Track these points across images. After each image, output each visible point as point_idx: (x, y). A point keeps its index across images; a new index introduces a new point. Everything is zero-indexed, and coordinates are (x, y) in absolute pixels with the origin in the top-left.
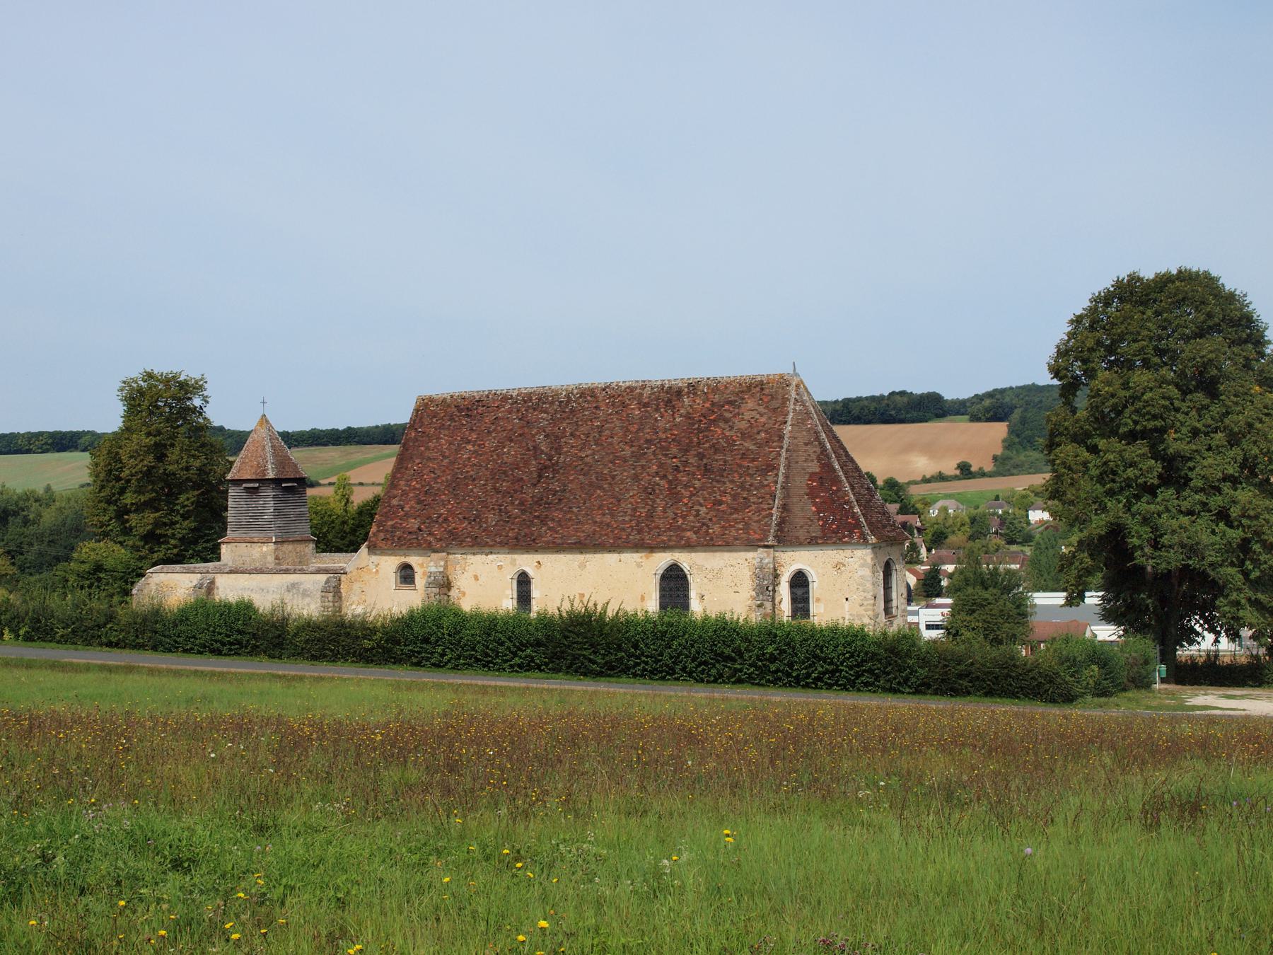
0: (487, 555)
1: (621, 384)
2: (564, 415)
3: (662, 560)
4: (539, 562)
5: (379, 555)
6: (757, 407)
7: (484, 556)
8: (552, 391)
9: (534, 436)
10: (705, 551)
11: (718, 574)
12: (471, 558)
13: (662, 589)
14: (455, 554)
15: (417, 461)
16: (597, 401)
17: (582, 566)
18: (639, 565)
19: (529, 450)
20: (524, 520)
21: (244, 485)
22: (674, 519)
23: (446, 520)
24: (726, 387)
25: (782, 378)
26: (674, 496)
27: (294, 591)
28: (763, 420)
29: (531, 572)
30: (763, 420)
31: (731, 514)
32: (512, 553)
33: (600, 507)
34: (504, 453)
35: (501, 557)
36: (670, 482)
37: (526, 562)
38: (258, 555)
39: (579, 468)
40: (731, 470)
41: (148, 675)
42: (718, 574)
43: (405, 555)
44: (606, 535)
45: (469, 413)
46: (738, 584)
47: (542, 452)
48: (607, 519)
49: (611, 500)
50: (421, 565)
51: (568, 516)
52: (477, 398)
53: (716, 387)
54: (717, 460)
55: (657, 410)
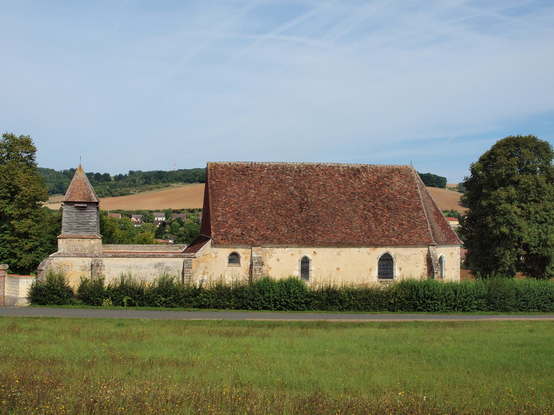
0: (285, 248)
1: (325, 164)
2: (301, 178)
3: (381, 251)
4: (315, 252)
5: (218, 247)
6: (401, 180)
7: (283, 249)
8: (288, 165)
9: (288, 187)
10: (403, 247)
11: (408, 258)
12: (276, 250)
13: (379, 265)
14: (265, 247)
15: (224, 197)
16: (316, 172)
17: (339, 254)
18: (369, 254)
19: (288, 194)
20: (303, 230)
21: (76, 205)
22: (383, 232)
23: (257, 229)
24: (381, 170)
25: (407, 167)
26: (377, 220)
27: (160, 267)
28: (406, 186)
29: (310, 256)
30: (406, 186)
31: (410, 230)
32: (300, 247)
33: (342, 225)
34: (275, 195)
35: (293, 249)
36: (373, 214)
37: (308, 252)
38: (87, 246)
39: (321, 205)
40: (401, 209)
41: (317, 328)
42: (408, 258)
43: (234, 248)
44: (352, 239)
45: (244, 173)
46: (418, 263)
47: (297, 196)
48: (349, 231)
49: (346, 222)
50: (244, 253)
51: (327, 229)
52: (245, 166)
53: (376, 170)
54: (391, 204)
55: (350, 178)
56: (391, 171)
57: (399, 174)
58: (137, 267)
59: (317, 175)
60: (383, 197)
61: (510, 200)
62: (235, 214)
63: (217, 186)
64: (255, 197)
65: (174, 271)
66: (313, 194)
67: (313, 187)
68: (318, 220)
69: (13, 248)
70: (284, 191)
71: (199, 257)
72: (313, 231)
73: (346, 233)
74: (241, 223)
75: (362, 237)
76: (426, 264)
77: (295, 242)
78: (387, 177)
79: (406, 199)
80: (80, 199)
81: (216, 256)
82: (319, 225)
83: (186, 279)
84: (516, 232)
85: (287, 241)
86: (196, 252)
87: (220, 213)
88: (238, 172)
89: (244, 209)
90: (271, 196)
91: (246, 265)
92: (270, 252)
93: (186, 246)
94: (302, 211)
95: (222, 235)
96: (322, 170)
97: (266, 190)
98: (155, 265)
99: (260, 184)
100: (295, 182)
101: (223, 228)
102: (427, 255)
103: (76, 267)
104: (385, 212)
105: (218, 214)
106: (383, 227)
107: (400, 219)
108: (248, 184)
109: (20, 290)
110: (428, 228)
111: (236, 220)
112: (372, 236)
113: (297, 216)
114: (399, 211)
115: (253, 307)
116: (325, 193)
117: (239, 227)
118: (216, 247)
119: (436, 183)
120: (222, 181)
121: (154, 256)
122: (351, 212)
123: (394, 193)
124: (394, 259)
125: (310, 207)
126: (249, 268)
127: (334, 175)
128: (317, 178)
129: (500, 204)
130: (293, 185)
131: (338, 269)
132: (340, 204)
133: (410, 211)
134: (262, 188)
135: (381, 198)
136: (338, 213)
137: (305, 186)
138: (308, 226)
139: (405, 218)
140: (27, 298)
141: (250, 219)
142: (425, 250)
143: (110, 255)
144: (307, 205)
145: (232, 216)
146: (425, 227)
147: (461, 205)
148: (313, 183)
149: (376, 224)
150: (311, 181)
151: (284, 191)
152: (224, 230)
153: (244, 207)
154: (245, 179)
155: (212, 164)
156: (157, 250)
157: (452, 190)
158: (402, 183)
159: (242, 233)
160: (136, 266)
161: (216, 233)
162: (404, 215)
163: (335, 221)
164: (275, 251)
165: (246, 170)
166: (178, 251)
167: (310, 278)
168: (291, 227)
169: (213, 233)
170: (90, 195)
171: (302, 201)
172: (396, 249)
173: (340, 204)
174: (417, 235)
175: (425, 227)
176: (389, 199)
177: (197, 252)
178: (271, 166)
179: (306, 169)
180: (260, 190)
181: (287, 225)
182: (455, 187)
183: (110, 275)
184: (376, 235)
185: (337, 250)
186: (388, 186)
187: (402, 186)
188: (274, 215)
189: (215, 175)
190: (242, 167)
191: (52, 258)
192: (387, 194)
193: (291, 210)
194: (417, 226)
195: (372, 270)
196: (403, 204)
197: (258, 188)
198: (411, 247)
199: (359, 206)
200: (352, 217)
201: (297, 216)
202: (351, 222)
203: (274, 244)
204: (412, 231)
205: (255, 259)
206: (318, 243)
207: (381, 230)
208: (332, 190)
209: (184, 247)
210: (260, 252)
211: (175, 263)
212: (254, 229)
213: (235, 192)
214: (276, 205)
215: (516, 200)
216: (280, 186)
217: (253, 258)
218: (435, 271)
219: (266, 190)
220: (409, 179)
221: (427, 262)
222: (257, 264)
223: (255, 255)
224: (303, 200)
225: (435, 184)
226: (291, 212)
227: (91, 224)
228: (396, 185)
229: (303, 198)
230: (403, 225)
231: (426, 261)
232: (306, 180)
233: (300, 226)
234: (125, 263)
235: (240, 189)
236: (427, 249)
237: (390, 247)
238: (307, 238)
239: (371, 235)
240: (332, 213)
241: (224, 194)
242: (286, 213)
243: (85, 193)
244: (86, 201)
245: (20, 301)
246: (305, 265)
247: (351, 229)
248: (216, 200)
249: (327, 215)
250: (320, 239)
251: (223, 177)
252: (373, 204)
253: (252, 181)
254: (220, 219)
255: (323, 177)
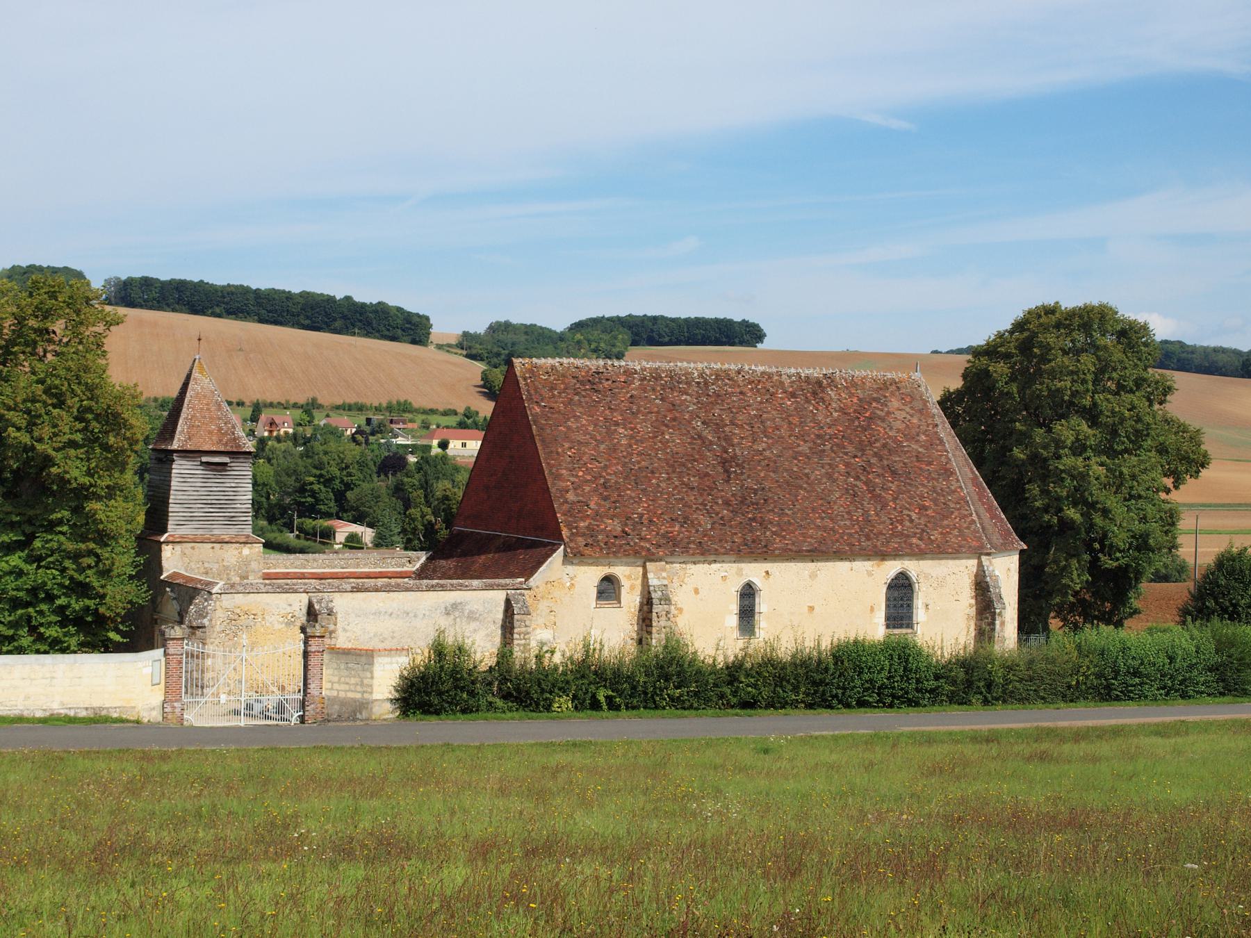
0: (710, 563)
3: (892, 568)
4: (767, 573)
5: (576, 564)
7: (706, 566)
9: (690, 422)
10: (932, 559)
12: (693, 569)
14: (672, 563)
15: (567, 445)
16: (739, 386)
17: (813, 576)
19: (692, 438)
20: (741, 523)
21: (204, 459)
24: (864, 383)
26: (876, 498)
27: (457, 614)
29: (758, 582)
32: (739, 562)
34: (668, 441)
36: (865, 483)
37: (753, 572)
38: (233, 561)
43: (609, 565)
44: (837, 541)
47: (711, 443)
49: (820, 502)
50: (629, 577)
54: (896, 462)
55: (807, 401)
56: (882, 386)
58: (408, 614)
59: (741, 393)
60: (878, 445)
61: (1079, 448)
62: (599, 487)
63: (548, 419)
64: (631, 446)
65: (486, 621)
66: (742, 438)
67: (740, 423)
68: (765, 500)
69: (81, 570)
70: (685, 432)
71: (537, 587)
73: (824, 529)
74: (616, 508)
75: (856, 536)
76: (973, 594)
77: (731, 550)
78: (877, 400)
79: (920, 450)
80: (213, 444)
81: (573, 584)
82: (770, 511)
83: (517, 639)
84: (1098, 520)
85: (716, 547)
86: (531, 574)
87: (569, 483)
88: (583, 383)
89: (615, 473)
90: (660, 442)
91: (632, 605)
92: (681, 573)
93: (423, 557)
94: (729, 477)
95: (583, 535)
96: (751, 382)
97: (648, 428)
98: (446, 608)
99: (633, 413)
100: (700, 408)
101: (583, 519)
102: (976, 576)
103: (273, 617)
104: (888, 481)
105: (564, 484)
106: (889, 513)
107: (918, 495)
108: (607, 412)
109: (375, 682)
110: (971, 515)
111: (606, 499)
112: (875, 534)
113: (722, 491)
114: (912, 476)
115: (840, 702)
116: (766, 436)
117: (614, 516)
118: (572, 564)
119: (403, 330)
121: (442, 586)
122: (824, 480)
123: (896, 437)
124: (917, 585)
125: (744, 468)
126: (637, 608)
128: (742, 399)
129: (1059, 457)
130: (697, 416)
131: (811, 608)
132: (799, 461)
133: (933, 479)
134: (639, 423)
135: (875, 447)
136: (800, 482)
137: (722, 420)
140: (391, 700)
141: (631, 497)
142: (972, 564)
143: (349, 589)
144: (737, 465)
145: (595, 490)
147: (484, 394)
148: (737, 413)
150: (734, 407)
151: (685, 432)
152: (587, 524)
153: (614, 469)
155: (523, 365)
156: (358, 566)
157: (448, 351)
158: (907, 413)
159: (623, 531)
160: (405, 612)
161: (570, 530)
162: (923, 485)
163: (798, 500)
164: (691, 572)
165: (597, 380)
166: (405, 569)
167: (757, 630)
168: (717, 514)
169: (565, 533)
170: (233, 434)
171: (725, 455)
172: (921, 562)
173: (799, 461)
174: (956, 532)
175: (966, 513)
177: (535, 576)
178: (645, 370)
179: (717, 379)
180: (635, 428)
181: (707, 509)
182: (453, 342)
183: (348, 634)
184: (881, 533)
185: (811, 566)
186: (883, 420)
187: (909, 421)
188: (676, 486)
189: (536, 389)
190: (588, 372)
191: (219, 596)
192: (885, 439)
193: (707, 475)
194: (952, 512)
196: (918, 461)
197: (630, 423)
198: (947, 558)
199: (837, 466)
200: (829, 491)
201: (722, 491)
202: (829, 503)
203: (693, 555)
204: (946, 522)
205: (655, 591)
206: (777, 552)
207: (888, 522)
208: (778, 429)
209: (419, 558)
210: (664, 574)
211: (488, 603)
213: (586, 432)
214: (675, 464)
215: (1091, 448)
216: (674, 419)
217: (652, 588)
218: (998, 611)
219: (648, 428)
220: (918, 405)
221: (976, 589)
222: (662, 602)
223: (653, 581)
224: (726, 452)
225: (399, 332)
226: (708, 480)
227: (239, 506)
228: (896, 418)
229: (724, 447)
230: (926, 510)
231: (973, 587)
232: (723, 406)
233: (732, 512)
234: (381, 605)
235: (596, 425)
236: (975, 562)
237: (908, 558)
238: (753, 541)
239: (871, 531)
241: (567, 438)
242: (700, 484)
244: (229, 449)
245: (377, 708)
247: (832, 519)
248: (552, 452)
249: (779, 486)
251: (554, 396)
252: (863, 461)
253: (615, 405)
254: (571, 496)
255: (754, 399)
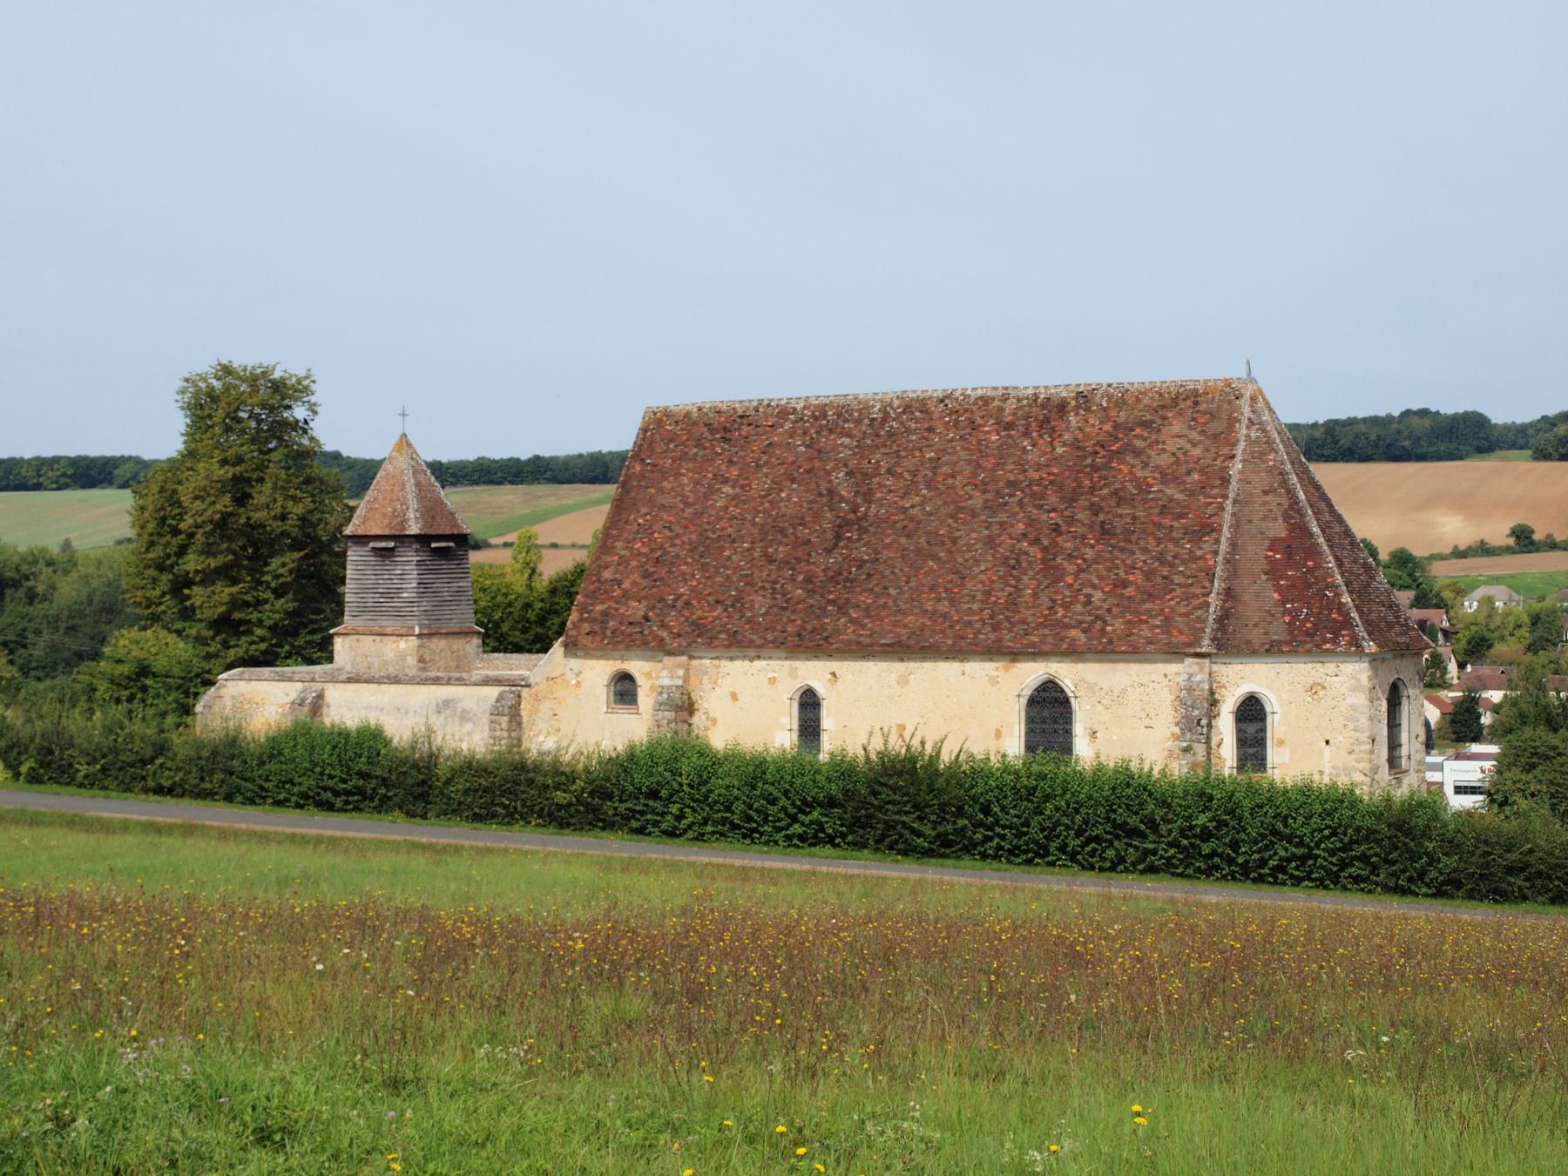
0: (751, 660)
1: (969, 392)
2: (878, 441)
3: (1031, 674)
4: (834, 674)
6: (1187, 432)
7: (747, 663)
8: (859, 402)
9: (829, 473)
10: (1100, 661)
12: (727, 665)
13: (1030, 720)
14: (701, 658)
15: (644, 510)
17: (903, 681)
18: (993, 681)
19: (820, 495)
20: (812, 606)
21: (372, 545)
23: (688, 603)
27: (448, 712)
28: (1197, 452)
29: (821, 689)
30: (1197, 452)
31: (1143, 602)
34: (782, 500)
35: (774, 664)
36: (1045, 550)
37: (814, 673)
39: (899, 525)
42: (1120, 698)
43: (622, 659)
46: (1152, 715)
47: (842, 499)
48: (944, 607)
50: (648, 675)
52: (740, 412)
53: (1121, 399)
54: (1121, 516)
57: (1189, 412)
60: (1105, 492)
72: (840, 608)
85: (755, 637)
92: (713, 672)
110: (1207, 595)
120: (661, 462)
127: (980, 426)
135: (1096, 496)
138: (831, 592)
139: (1145, 561)
146: (1199, 591)
149: (1039, 585)
154: (720, 454)
176: (1120, 499)
184: (1024, 621)
186: (1137, 453)
195: (1004, 734)
198: (1128, 661)
204: (1148, 606)
212: (679, 604)
216: (808, 472)
220: (1216, 427)
230: (1125, 587)
235: (697, 483)
239: (1008, 618)
240: (918, 551)
243: (395, 510)
246: (810, 715)
250: (850, 633)
